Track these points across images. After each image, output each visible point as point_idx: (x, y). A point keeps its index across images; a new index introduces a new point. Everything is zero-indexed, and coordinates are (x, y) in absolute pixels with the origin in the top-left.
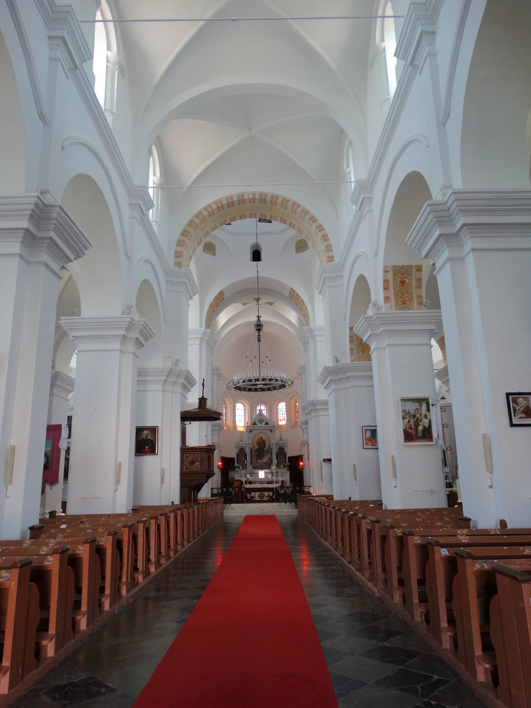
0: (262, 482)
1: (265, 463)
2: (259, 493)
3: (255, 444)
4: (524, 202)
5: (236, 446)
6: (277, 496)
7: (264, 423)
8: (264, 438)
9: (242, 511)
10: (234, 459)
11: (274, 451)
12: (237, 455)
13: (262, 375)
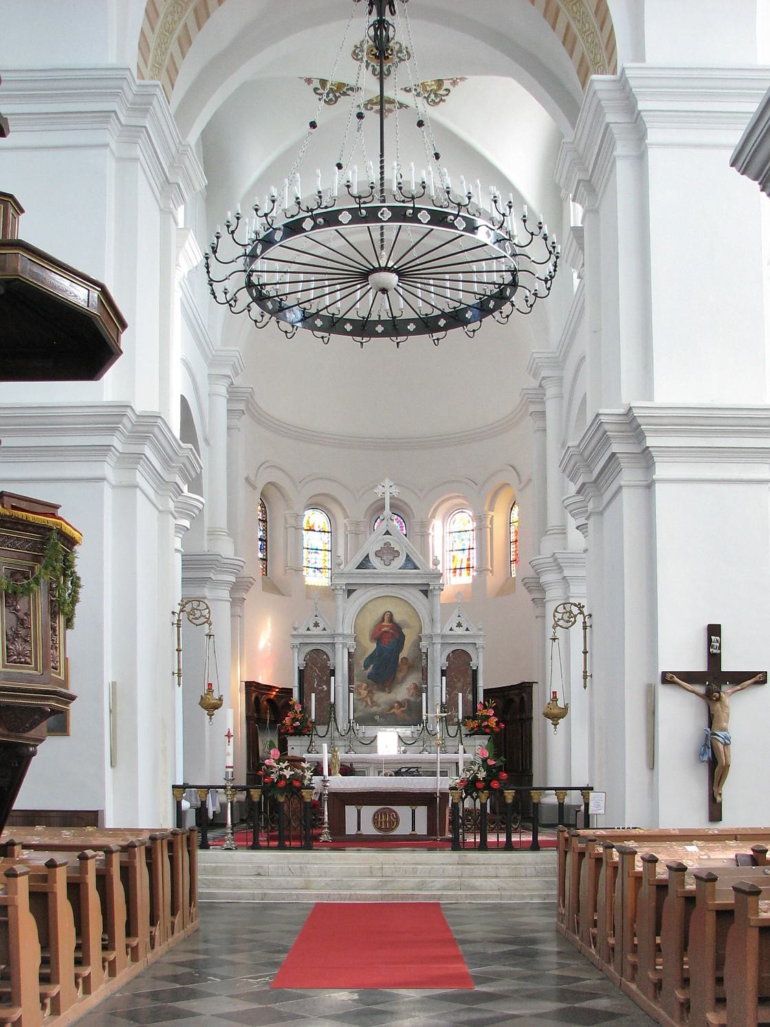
0: (381, 767)
1: (400, 704)
2: (375, 808)
3: (367, 637)
4: (42, 85)
5: (297, 641)
6: (448, 825)
7: (401, 560)
8: (398, 618)
9: (297, 881)
10: (289, 692)
11: (438, 660)
12: (301, 673)
13: (391, 176)
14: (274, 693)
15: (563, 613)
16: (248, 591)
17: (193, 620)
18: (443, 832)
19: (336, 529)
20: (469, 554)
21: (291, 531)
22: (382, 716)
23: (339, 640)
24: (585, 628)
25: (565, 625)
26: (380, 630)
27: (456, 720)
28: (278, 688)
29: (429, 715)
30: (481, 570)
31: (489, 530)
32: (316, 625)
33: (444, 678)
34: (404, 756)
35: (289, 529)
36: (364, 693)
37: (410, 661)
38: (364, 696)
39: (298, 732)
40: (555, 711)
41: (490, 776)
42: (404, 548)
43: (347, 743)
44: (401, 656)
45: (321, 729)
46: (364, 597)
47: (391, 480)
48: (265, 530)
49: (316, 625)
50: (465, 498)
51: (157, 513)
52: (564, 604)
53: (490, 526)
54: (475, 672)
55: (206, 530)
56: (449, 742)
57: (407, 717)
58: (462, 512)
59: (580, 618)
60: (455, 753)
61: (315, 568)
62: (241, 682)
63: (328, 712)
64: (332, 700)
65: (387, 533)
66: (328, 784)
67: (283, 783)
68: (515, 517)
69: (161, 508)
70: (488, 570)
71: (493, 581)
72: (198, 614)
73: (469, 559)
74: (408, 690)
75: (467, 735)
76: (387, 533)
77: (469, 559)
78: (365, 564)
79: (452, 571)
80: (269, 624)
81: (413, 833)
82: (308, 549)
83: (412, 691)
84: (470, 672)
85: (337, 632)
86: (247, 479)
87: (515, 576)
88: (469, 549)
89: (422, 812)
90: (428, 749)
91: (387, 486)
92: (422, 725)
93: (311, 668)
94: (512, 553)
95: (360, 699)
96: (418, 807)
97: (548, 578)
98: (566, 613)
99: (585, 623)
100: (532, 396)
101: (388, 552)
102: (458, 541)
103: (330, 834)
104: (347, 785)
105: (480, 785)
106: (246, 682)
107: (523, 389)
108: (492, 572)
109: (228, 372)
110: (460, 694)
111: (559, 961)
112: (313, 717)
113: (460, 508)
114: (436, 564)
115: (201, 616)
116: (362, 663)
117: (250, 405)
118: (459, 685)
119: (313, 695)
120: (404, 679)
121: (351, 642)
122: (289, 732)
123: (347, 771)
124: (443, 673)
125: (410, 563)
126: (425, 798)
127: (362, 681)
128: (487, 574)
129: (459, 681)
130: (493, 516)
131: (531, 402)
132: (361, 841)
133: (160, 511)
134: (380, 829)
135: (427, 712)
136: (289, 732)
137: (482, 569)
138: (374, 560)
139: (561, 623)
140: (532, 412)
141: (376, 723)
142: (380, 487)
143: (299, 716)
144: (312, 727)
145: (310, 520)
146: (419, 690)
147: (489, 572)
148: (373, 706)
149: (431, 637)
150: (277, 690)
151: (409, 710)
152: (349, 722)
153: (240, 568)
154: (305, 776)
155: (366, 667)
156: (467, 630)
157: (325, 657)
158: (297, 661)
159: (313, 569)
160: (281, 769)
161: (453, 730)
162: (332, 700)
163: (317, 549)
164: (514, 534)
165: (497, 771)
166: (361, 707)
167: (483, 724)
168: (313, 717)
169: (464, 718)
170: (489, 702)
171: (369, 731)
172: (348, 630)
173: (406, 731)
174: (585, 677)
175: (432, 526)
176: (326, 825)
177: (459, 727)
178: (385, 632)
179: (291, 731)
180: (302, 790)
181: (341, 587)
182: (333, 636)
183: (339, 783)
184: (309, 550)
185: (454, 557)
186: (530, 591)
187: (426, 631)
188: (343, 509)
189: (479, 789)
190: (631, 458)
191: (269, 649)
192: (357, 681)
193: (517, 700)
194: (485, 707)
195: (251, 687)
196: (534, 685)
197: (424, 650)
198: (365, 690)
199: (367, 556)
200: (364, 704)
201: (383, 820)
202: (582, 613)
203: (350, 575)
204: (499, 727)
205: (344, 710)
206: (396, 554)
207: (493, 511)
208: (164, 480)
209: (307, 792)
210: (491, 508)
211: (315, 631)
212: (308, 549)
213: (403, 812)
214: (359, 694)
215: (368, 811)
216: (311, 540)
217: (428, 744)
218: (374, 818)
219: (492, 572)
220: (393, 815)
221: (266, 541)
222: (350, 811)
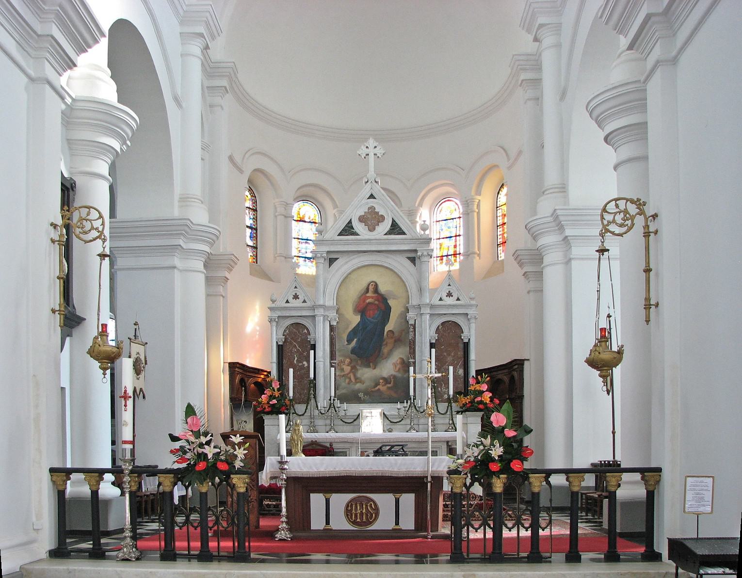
1: (386, 381)
5: (276, 314)
7: (386, 226)
8: (383, 289)
11: (427, 332)
12: (280, 349)
14: (262, 376)
15: (615, 213)
16: (231, 270)
17: (81, 236)
18: (435, 527)
19: (326, 220)
20: (456, 241)
21: (280, 219)
22: (366, 393)
23: (319, 312)
24: (647, 235)
25: (617, 230)
26: (364, 301)
27: (446, 396)
28: (266, 371)
29: (418, 376)
30: (468, 254)
31: (475, 214)
32: (296, 297)
33: (433, 350)
34: (389, 435)
35: (279, 217)
36: (347, 369)
37: (396, 334)
38: (346, 373)
39: (276, 411)
40: (605, 356)
41: (510, 453)
42: (389, 212)
43: (328, 422)
44: (388, 328)
45: (300, 408)
46: (346, 267)
47: (376, 140)
48: (255, 219)
49: (296, 297)
50: (452, 185)
51: (25, 80)
52: (616, 200)
53: (477, 211)
54: (466, 346)
55: (176, 198)
56: (440, 420)
57: (395, 395)
58: (449, 200)
59: (640, 221)
60: (446, 431)
61: (305, 258)
62: (224, 363)
63: (308, 388)
64: (312, 376)
65: (372, 196)
66: (286, 466)
67: (202, 466)
68: (502, 199)
69: (31, 72)
70: (475, 253)
71: (480, 264)
72: (88, 226)
73: (455, 246)
74: (395, 365)
75: (458, 412)
76: (372, 196)
77: (455, 246)
78: (348, 230)
79: (439, 258)
80: (257, 307)
81: (397, 527)
82: (298, 239)
83: (398, 367)
84: (461, 346)
85: (317, 303)
86: (231, 159)
87: (503, 258)
88: (456, 236)
89: (408, 500)
90: (416, 427)
91: (371, 147)
92: (409, 402)
93: (291, 343)
94: (499, 237)
95: (343, 376)
96: (403, 494)
97: (549, 239)
98: (620, 213)
99: (647, 226)
100: (522, 62)
101: (372, 219)
102: (445, 228)
103: (290, 530)
104: (311, 467)
105: (494, 467)
106: (230, 363)
107: (513, 55)
108: (479, 255)
109: (201, 29)
110: (451, 368)
111: (321, 336)
112: (291, 394)
113: (446, 198)
114: (424, 228)
115: (92, 228)
116: (345, 337)
117: (233, 84)
118: (450, 359)
119: (291, 371)
120: (390, 353)
121: (333, 314)
122: (265, 410)
123: (313, 449)
124: (432, 346)
125: (395, 228)
126: (413, 484)
127: (346, 357)
128: (474, 257)
129: (449, 355)
130: (480, 200)
131: (521, 69)
132: (330, 541)
133: (31, 79)
134: (354, 523)
135: (414, 372)
136: (265, 410)
137: (469, 253)
138: (358, 227)
139: (612, 228)
140: (523, 81)
141: (359, 401)
142: (364, 148)
143: (277, 394)
144: (290, 405)
145: (300, 211)
146: (405, 365)
147: (476, 256)
148: (356, 383)
149: (419, 307)
150: (265, 373)
151: (396, 387)
152: (330, 400)
153: (215, 238)
154: (236, 456)
155: (349, 341)
156: (458, 299)
157: (306, 331)
158: (277, 336)
159: (304, 259)
160: (201, 445)
161: (443, 407)
162: (312, 376)
163: (307, 240)
164: (501, 218)
165: (193, 510)
166: (343, 384)
167: (476, 400)
168: (291, 394)
169: (455, 393)
170: (482, 377)
171: (352, 409)
172: (330, 302)
173: (392, 409)
174: (648, 307)
175: (419, 214)
176: (284, 519)
177: (450, 402)
178: (369, 303)
179: (267, 410)
180: (232, 476)
181: (322, 254)
182: (313, 308)
183: (303, 465)
184: (299, 240)
185: (441, 245)
186: (521, 264)
187: (414, 301)
188: (332, 199)
189: (494, 473)
190: (535, 275)
191: (258, 333)
192: (340, 356)
193: (506, 379)
194: (478, 382)
195: (234, 367)
196: (526, 362)
197: (411, 322)
198: (348, 365)
199: (350, 222)
200: (347, 380)
201: (359, 511)
202: (641, 213)
203: (332, 242)
204: (494, 403)
205: (325, 387)
206: (382, 219)
207: (480, 195)
208: (35, 32)
209: (239, 479)
210: (479, 193)
211: (295, 303)
212: (298, 239)
213: (384, 501)
214: (342, 370)
215: (340, 500)
216: (298, 230)
217: (415, 422)
218: (347, 506)
219: (479, 255)
220: (371, 505)
221: (256, 229)
222: (317, 500)
